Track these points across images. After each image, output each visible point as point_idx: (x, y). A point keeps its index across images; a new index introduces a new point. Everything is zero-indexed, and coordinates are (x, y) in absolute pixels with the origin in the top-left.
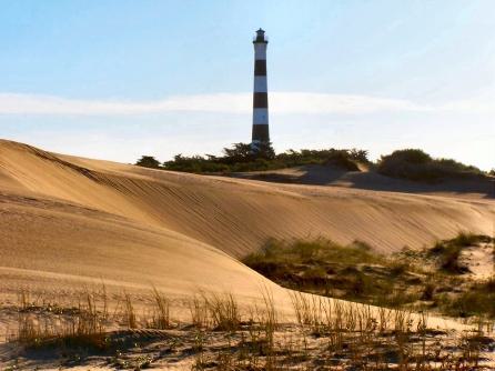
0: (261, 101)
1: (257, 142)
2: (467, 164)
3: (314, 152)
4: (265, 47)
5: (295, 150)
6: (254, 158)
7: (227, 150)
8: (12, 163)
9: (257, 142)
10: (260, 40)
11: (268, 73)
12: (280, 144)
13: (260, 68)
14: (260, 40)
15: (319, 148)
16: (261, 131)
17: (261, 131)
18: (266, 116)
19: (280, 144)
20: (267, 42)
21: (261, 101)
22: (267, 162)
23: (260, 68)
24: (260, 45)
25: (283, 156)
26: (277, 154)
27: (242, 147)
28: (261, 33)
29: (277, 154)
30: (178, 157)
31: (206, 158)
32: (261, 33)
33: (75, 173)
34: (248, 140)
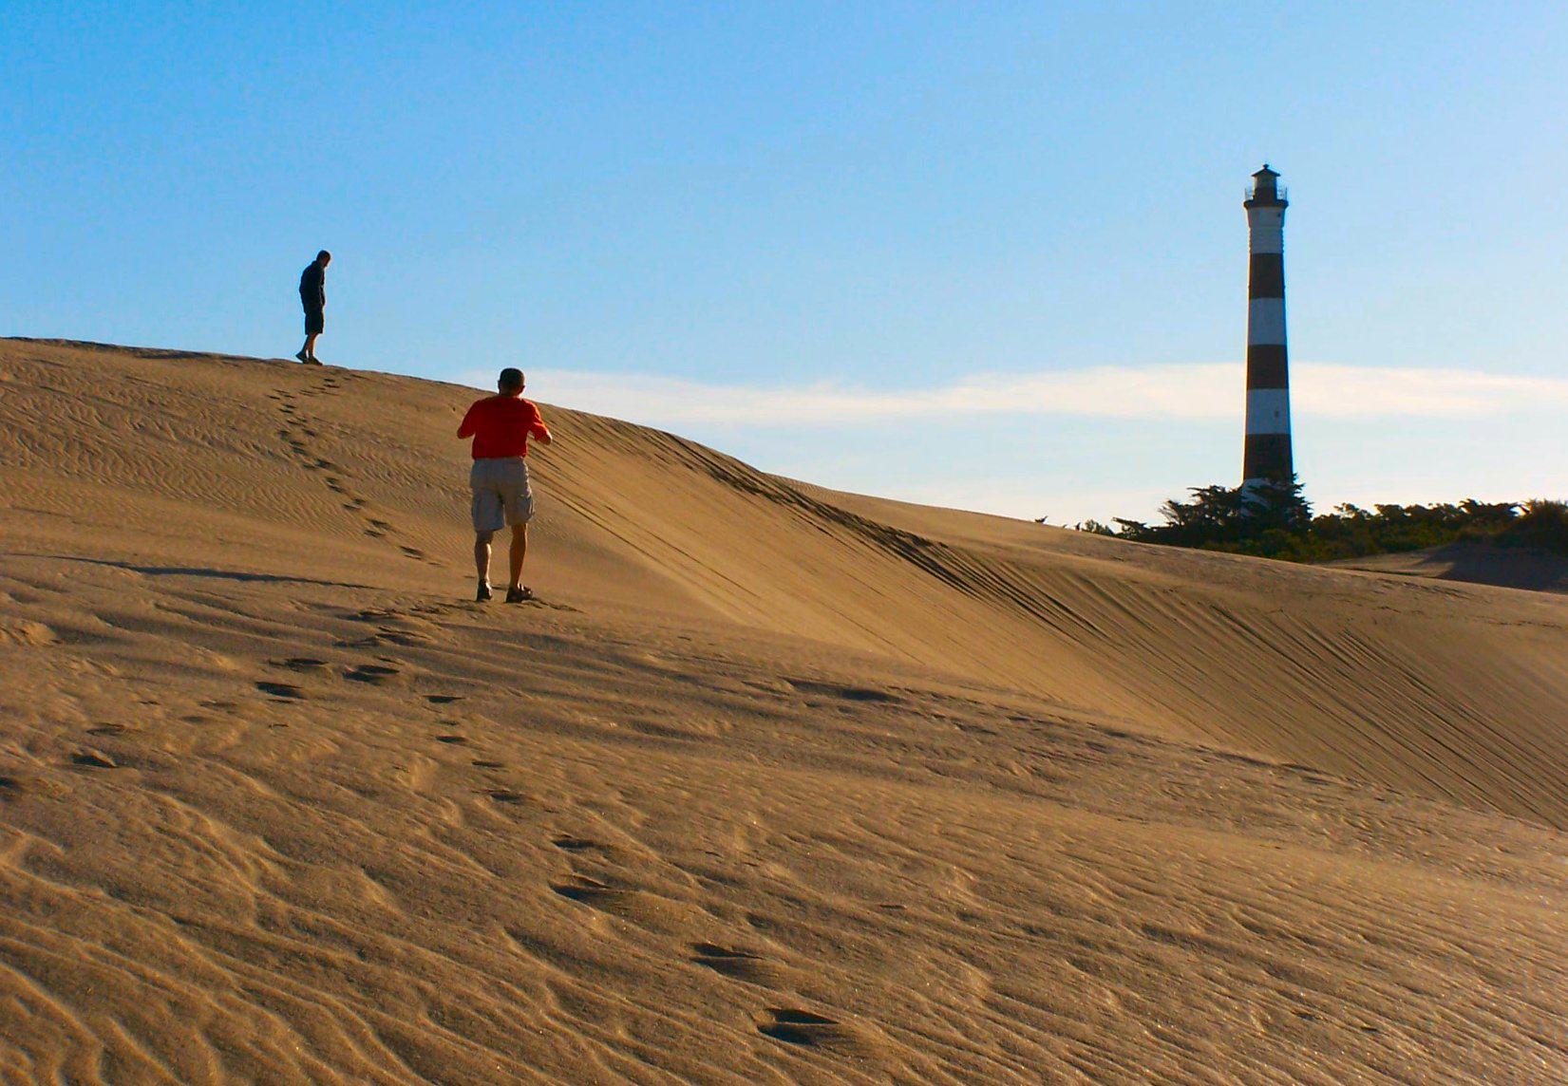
0: (1268, 368)
1: (1257, 482)
2: (1032, 517)
3: (1417, 510)
4: (1281, 215)
5: (1360, 506)
6: (1257, 512)
7: (1174, 506)
8: (622, 505)
9: (1257, 482)
10: (1266, 199)
11: (1288, 291)
12: (1326, 487)
13: (1267, 278)
14: (1266, 199)
15: (1428, 500)
16: (1269, 450)
17: (1269, 450)
18: (1282, 412)
19: (1326, 487)
20: (1284, 204)
21: (1268, 368)
22: (1291, 539)
23: (1267, 278)
24: (1265, 212)
25: (1329, 525)
26: (1317, 511)
27: (1214, 497)
28: (1266, 179)
29: (1317, 511)
30: (1248, 204)
31: (1375, 512)
32: (1266, 179)
33: (869, 550)
34: (1231, 477)
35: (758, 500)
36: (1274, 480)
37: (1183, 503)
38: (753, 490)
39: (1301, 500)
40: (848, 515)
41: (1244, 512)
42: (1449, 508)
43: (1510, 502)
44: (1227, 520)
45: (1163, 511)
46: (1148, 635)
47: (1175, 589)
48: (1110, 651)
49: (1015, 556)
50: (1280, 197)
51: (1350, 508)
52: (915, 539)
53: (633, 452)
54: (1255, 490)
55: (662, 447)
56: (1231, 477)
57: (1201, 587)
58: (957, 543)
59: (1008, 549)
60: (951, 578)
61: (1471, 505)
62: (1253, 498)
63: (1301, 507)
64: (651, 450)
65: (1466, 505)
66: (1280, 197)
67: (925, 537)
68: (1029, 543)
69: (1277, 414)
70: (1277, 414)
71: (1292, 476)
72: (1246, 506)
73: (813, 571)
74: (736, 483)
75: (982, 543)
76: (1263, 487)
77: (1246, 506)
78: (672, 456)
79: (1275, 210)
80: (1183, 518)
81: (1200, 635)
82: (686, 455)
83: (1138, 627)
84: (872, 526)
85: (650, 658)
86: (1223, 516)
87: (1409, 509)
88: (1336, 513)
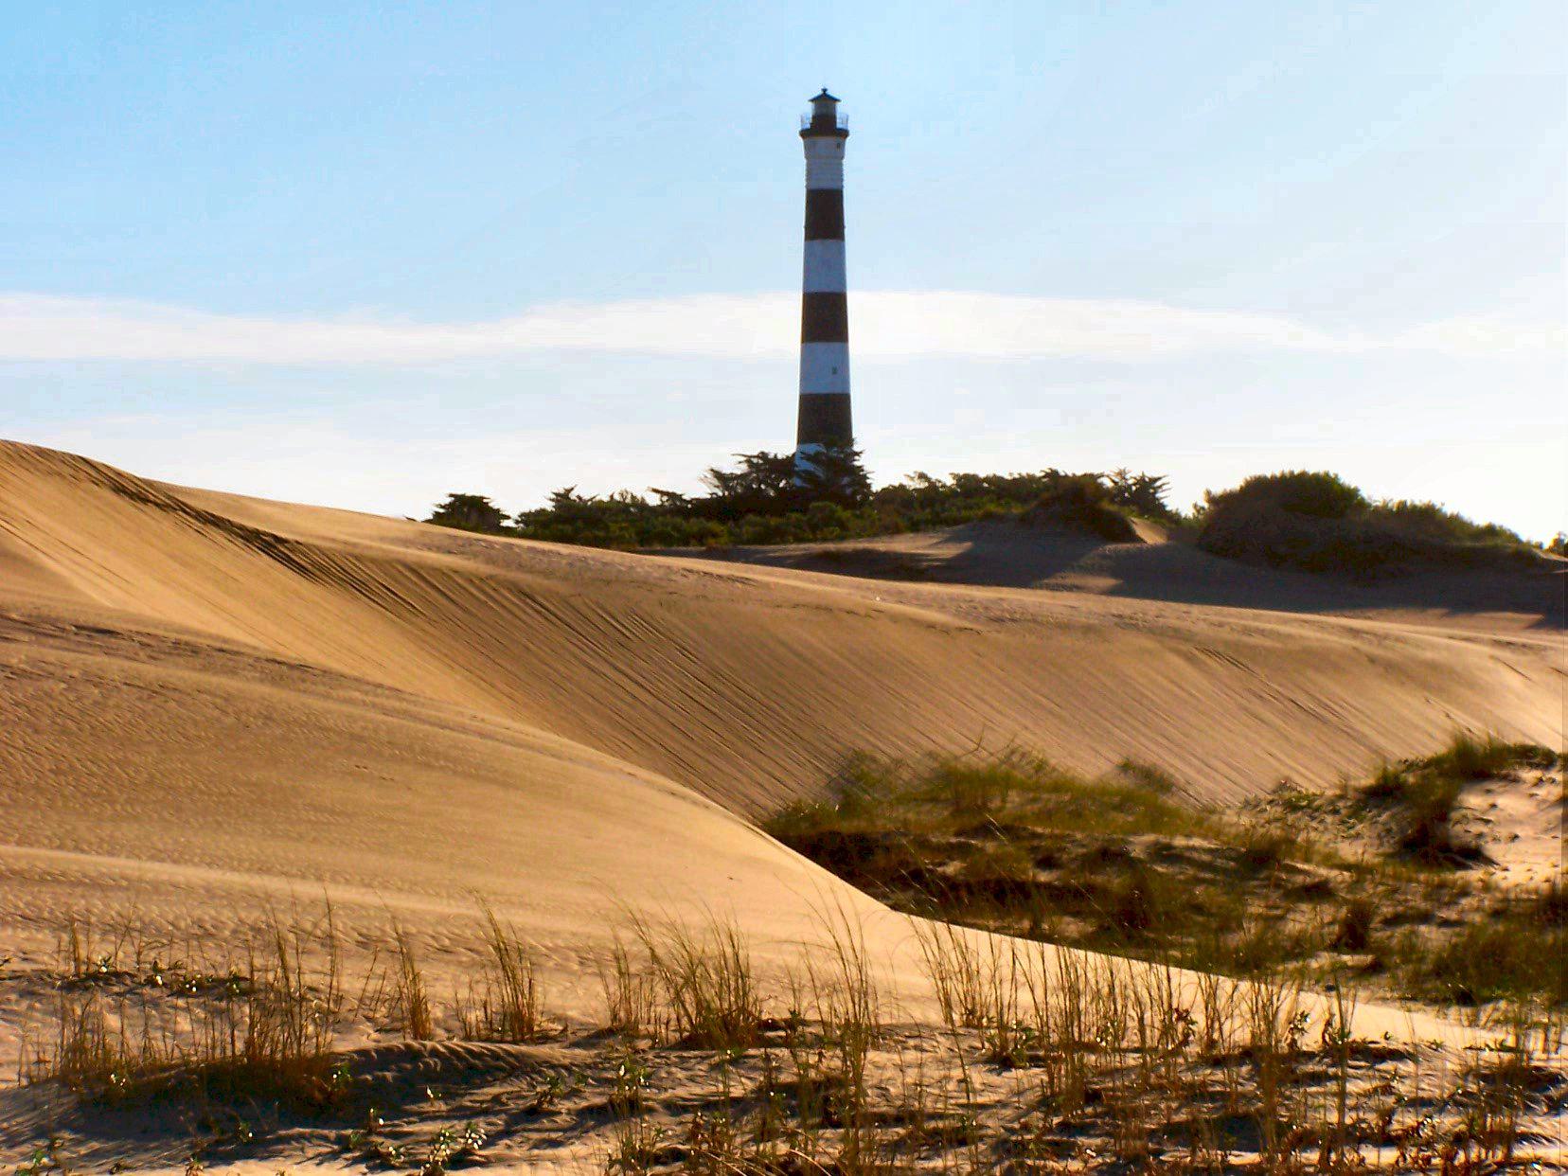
0: (825, 318)
1: (812, 448)
3: (996, 481)
4: (840, 146)
5: (933, 477)
8: (41, 519)
9: (812, 448)
10: (824, 127)
11: (847, 231)
12: (889, 455)
13: (825, 216)
14: (824, 127)
16: (825, 414)
17: (825, 414)
19: (889, 455)
20: (844, 133)
21: (825, 318)
23: (825, 216)
24: (824, 142)
25: (896, 496)
27: (766, 466)
28: (825, 104)
29: (877, 484)
30: (804, 134)
32: (825, 104)
33: (236, 549)
34: (784, 443)
35: (150, 509)
36: (829, 445)
37: (727, 470)
38: (146, 501)
39: (860, 468)
40: (222, 520)
41: (797, 481)
42: (1031, 479)
43: (1096, 472)
44: (780, 492)
45: (704, 480)
46: (460, 613)
47: (491, 577)
48: (427, 627)
49: (357, 551)
50: (839, 125)
51: (922, 476)
52: (275, 537)
53: (50, 473)
54: (808, 457)
55: (76, 469)
56: (784, 443)
57: (513, 575)
58: (311, 541)
59: (355, 545)
60: (301, 570)
61: (1053, 475)
62: (804, 465)
63: (859, 478)
64: (66, 470)
65: (1047, 475)
66: (839, 125)
67: (283, 535)
68: (382, 539)
69: (835, 371)
70: (835, 371)
71: (850, 441)
72: (798, 475)
73: (184, 564)
74: (132, 496)
75: (334, 540)
76: (818, 454)
77: (798, 475)
78: (82, 476)
79: (831, 140)
80: (726, 487)
81: (505, 614)
82: (93, 473)
83: (453, 607)
84: (242, 528)
85: (14, 616)
86: (776, 487)
87: (987, 479)
88: (907, 482)
